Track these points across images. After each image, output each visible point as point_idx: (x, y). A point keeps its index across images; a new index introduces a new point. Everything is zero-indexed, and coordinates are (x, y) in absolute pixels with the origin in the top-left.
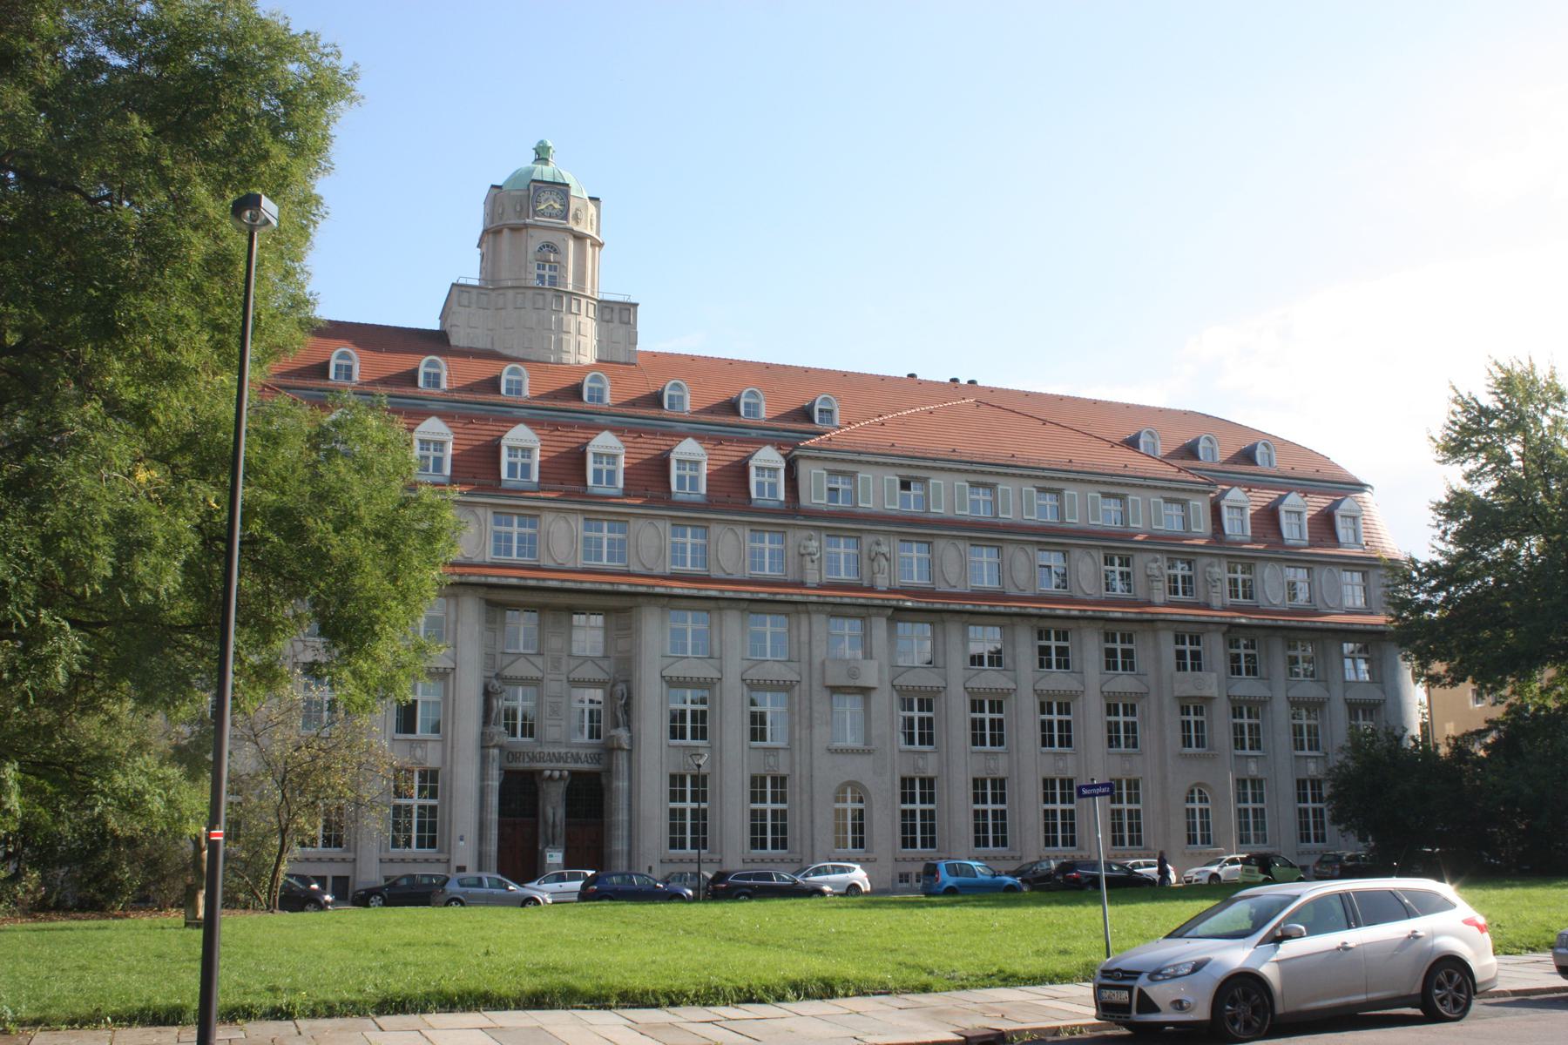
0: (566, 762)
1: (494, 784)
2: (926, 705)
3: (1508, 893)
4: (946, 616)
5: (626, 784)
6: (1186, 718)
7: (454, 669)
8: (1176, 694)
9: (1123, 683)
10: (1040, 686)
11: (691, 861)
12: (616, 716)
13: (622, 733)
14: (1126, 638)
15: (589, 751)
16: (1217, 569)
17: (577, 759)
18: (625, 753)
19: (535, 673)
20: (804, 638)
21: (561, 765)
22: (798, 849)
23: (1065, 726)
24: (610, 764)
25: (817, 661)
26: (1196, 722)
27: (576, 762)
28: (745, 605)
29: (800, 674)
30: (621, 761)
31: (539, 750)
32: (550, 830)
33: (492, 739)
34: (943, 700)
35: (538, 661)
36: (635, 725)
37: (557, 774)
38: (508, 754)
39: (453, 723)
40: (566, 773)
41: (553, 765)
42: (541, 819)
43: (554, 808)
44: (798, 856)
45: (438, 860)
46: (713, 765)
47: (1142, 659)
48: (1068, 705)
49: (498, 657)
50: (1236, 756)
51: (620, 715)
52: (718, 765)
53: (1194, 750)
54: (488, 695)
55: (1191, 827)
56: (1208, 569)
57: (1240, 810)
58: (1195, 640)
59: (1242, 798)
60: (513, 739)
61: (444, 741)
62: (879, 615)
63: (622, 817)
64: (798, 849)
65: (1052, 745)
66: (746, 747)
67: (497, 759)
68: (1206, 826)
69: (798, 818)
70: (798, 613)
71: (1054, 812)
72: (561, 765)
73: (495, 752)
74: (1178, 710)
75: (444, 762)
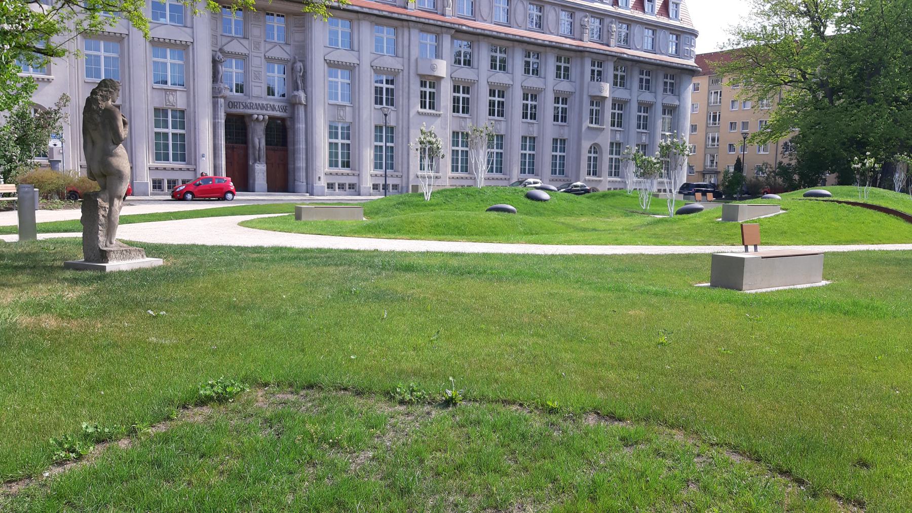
0: (267, 110)
1: (222, 121)
2: (466, 90)
3: (174, 205)
4: (481, 37)
5: (304, 126)
6: (423, 89)
7: (679, 106)
8: (590, 94)
9: (565, 86)
10: (524, 84)
11: (381, 175)
12: (297, 83)
13: (301, 94)
14: (568, 60)
15: (280, 104)
16: (614, 26)
17: (273, 108)
18: (303, 107)
19: (243, 51)
20: (406, 43)
21: (264, 112)
22: (400, 170)
23: (466, 101)
24: (293, 113)
25: (413, 59)
26: (430, 93)
27: (273, 110)
28: (373, 18)
29: (403, 66)
30: (301, 111)
31: (249, 101)
32: (257, 152)
33: (220, 92)
34: (543, 95)
35: (245, 42)
36: (309, 89)
37: (261, 117)
38: (231, 104)
39: (194, 80)
40: (267, 117)
41: (259, 111)
42: (250, 146)
43: (258, 139)
44: (400, 174)
45: (188, 170)
46: (507, 130)
47: (574, 72)
48: (468, 88)
49: (219, 38)
50: (638, 132)
51: (299, 82)
52: (357, 117)
53: (427, 111)
54: (215, 63)
55: (554, 165)
56: (610, 25)
57: (453, 151)
58: (600, 65)
59: (554, 149)
60: (231, 94)
61: (188, 92)
62: (446, 33)
63: (302, 146)
64: (400, 170)
65: (458, 112)
66: (373, 109)
67: (223, 105)
68: (532, 164)
69: (400, 152)
70: (403, 27)
71: (457, 151)
72: (264, 112)
73: (221, 101)
74: (419, 84)
75: (188, 105)
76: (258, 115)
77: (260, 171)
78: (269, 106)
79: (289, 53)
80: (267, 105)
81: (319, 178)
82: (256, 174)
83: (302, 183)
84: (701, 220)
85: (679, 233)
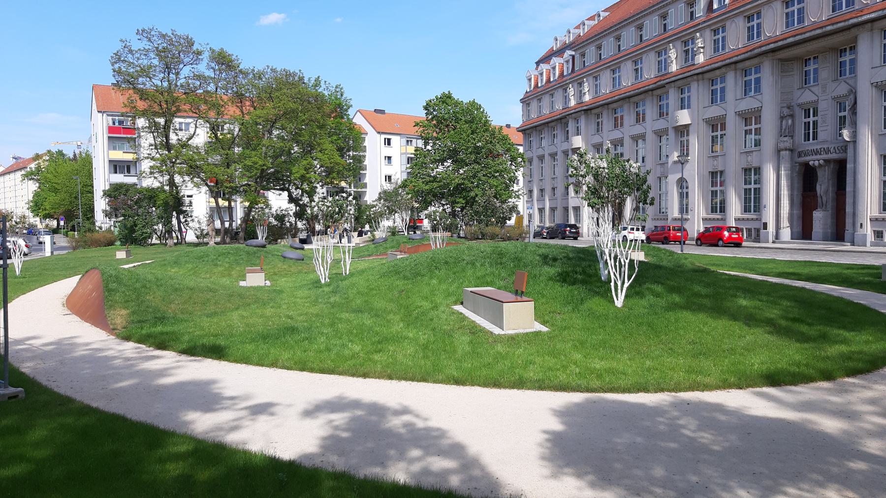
17: (827, 151)
21: (818, 157)
37: (816, 163)
41: (814, 157)
43: (824, 186)
76: (819, 160)
77: (820, 218)
78: (822, 150)
79: (838, 84)
80: (821, 149)
81: (861, 225)
82: (814, 222)
83: (847, 235)
84: (839, 332)
85: (695, 356)
